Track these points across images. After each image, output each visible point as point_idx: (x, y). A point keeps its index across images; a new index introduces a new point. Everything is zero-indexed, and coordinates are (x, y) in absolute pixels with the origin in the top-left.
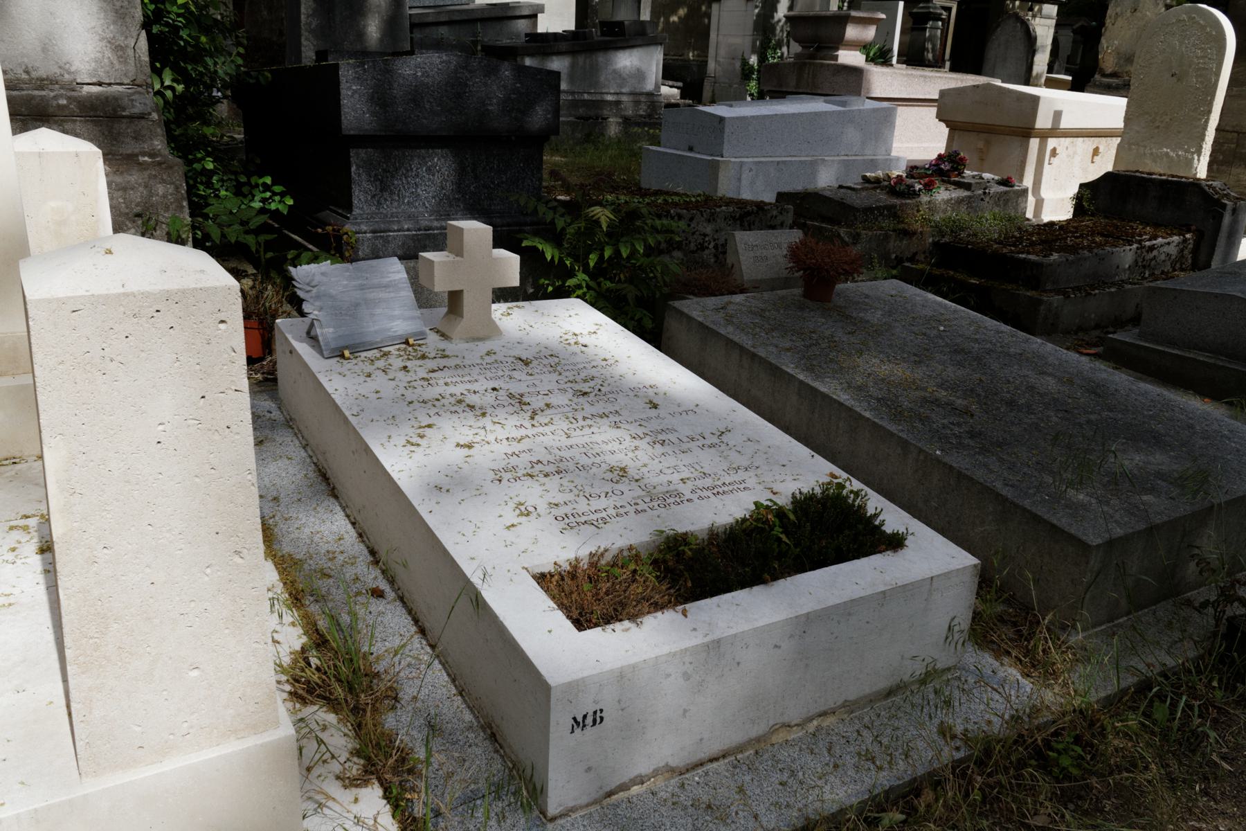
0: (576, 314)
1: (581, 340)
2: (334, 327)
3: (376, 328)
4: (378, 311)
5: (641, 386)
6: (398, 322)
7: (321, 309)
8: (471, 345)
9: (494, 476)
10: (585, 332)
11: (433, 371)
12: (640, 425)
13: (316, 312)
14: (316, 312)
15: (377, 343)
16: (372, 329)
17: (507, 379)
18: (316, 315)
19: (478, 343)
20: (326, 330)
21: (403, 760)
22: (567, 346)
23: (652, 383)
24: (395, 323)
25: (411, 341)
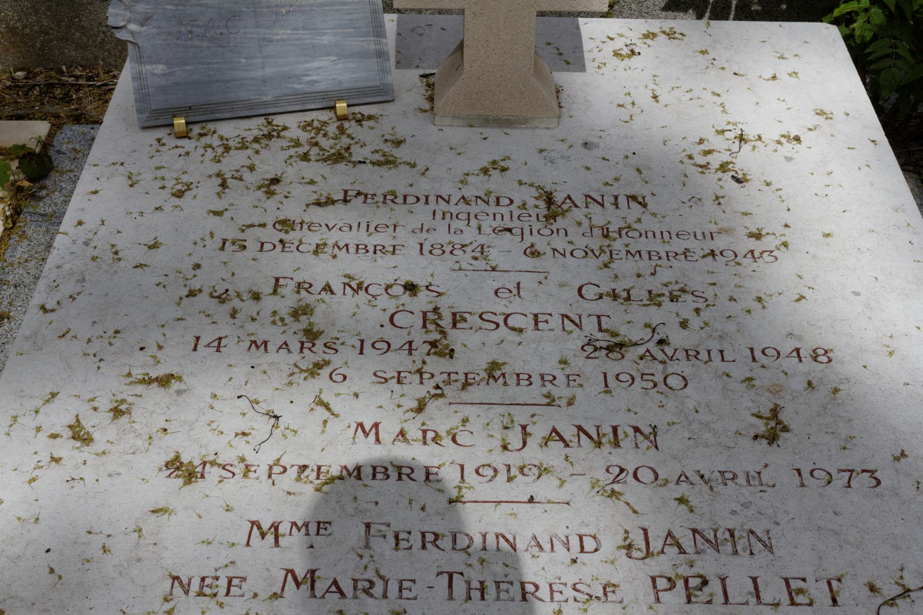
0: (795, 74)
1: (746, 160)
2: (167, 63)
3: (269, 71)
4: (282, 33)
5: (787, 347)
6: (324, 62)
7: (145, 21)
8: (474, 134)
9: (612, 243)
10: (772, 133)
11: (326, 202)
12: (681, 500)
13: (133, 27)
14: (133, 27)
15: (265, 104)
16: (259, 73)
17: (465, 259)
18: (133, 33)
19: (487, 132)
20: (148, 67)
21: (428, 474)
22: (693, 171)
23: (826, 340)
24: (316, 64)
25: (341, 106)
